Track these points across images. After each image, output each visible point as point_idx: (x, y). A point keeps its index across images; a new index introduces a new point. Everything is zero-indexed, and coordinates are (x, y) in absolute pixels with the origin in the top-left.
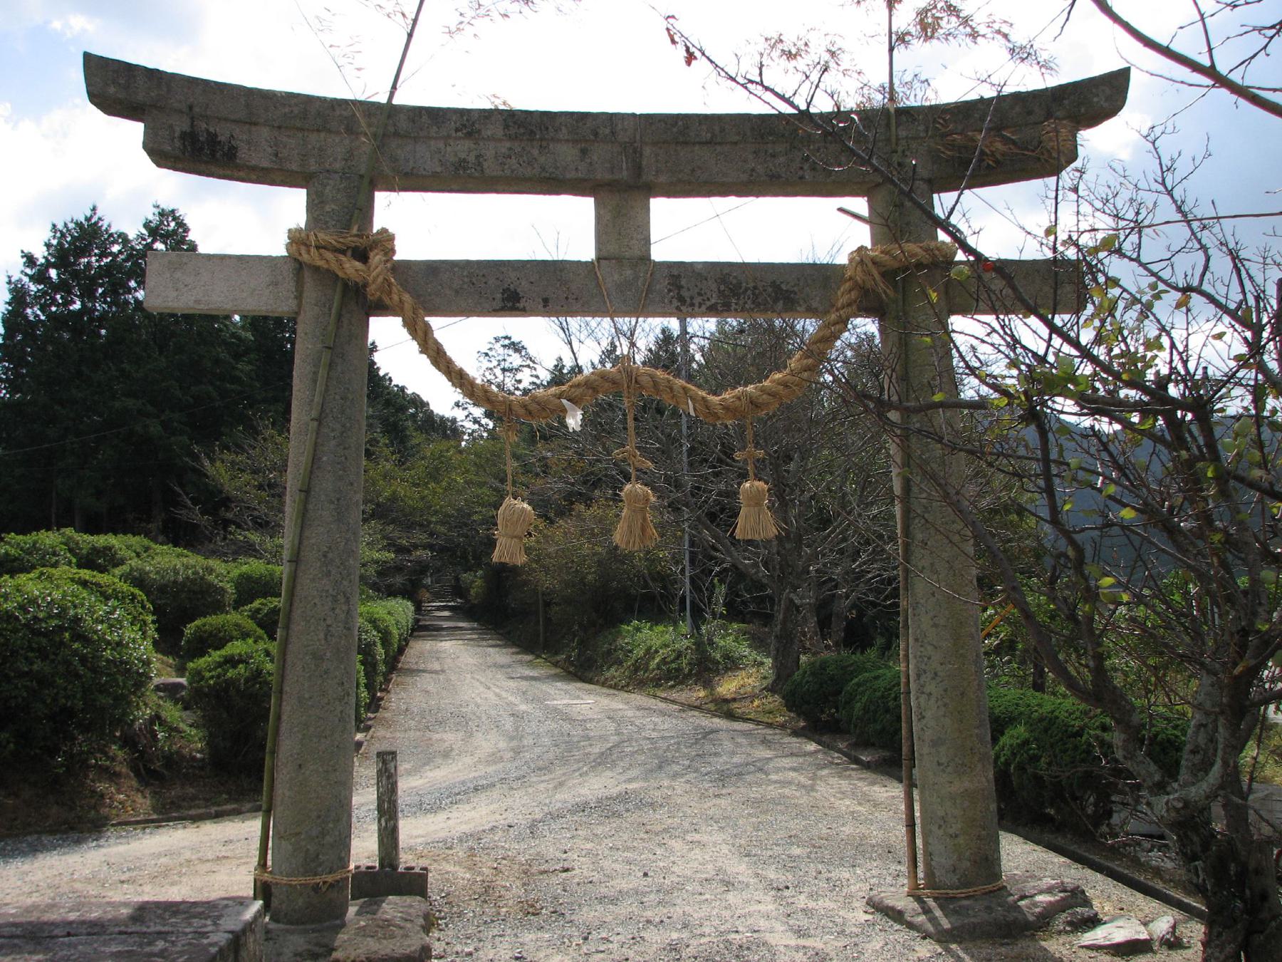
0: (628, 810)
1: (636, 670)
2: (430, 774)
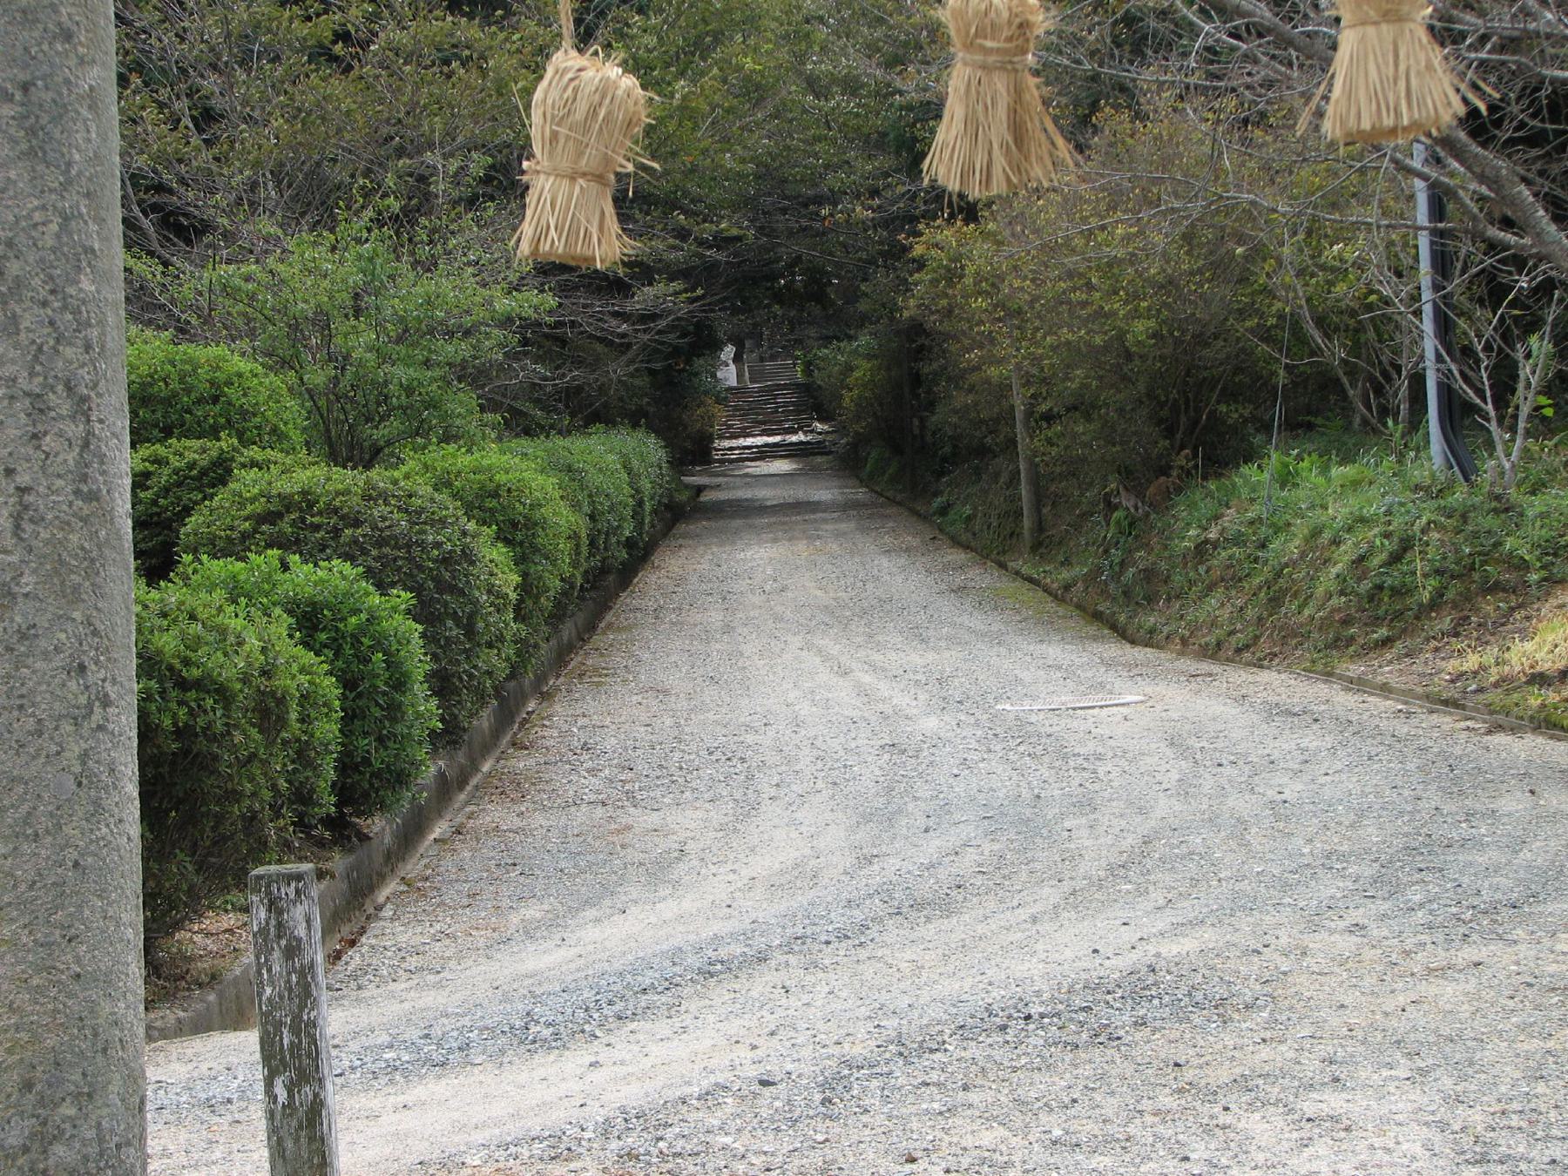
0: (1141, 1023)
1: (1275, 602)
2: (592, 933)
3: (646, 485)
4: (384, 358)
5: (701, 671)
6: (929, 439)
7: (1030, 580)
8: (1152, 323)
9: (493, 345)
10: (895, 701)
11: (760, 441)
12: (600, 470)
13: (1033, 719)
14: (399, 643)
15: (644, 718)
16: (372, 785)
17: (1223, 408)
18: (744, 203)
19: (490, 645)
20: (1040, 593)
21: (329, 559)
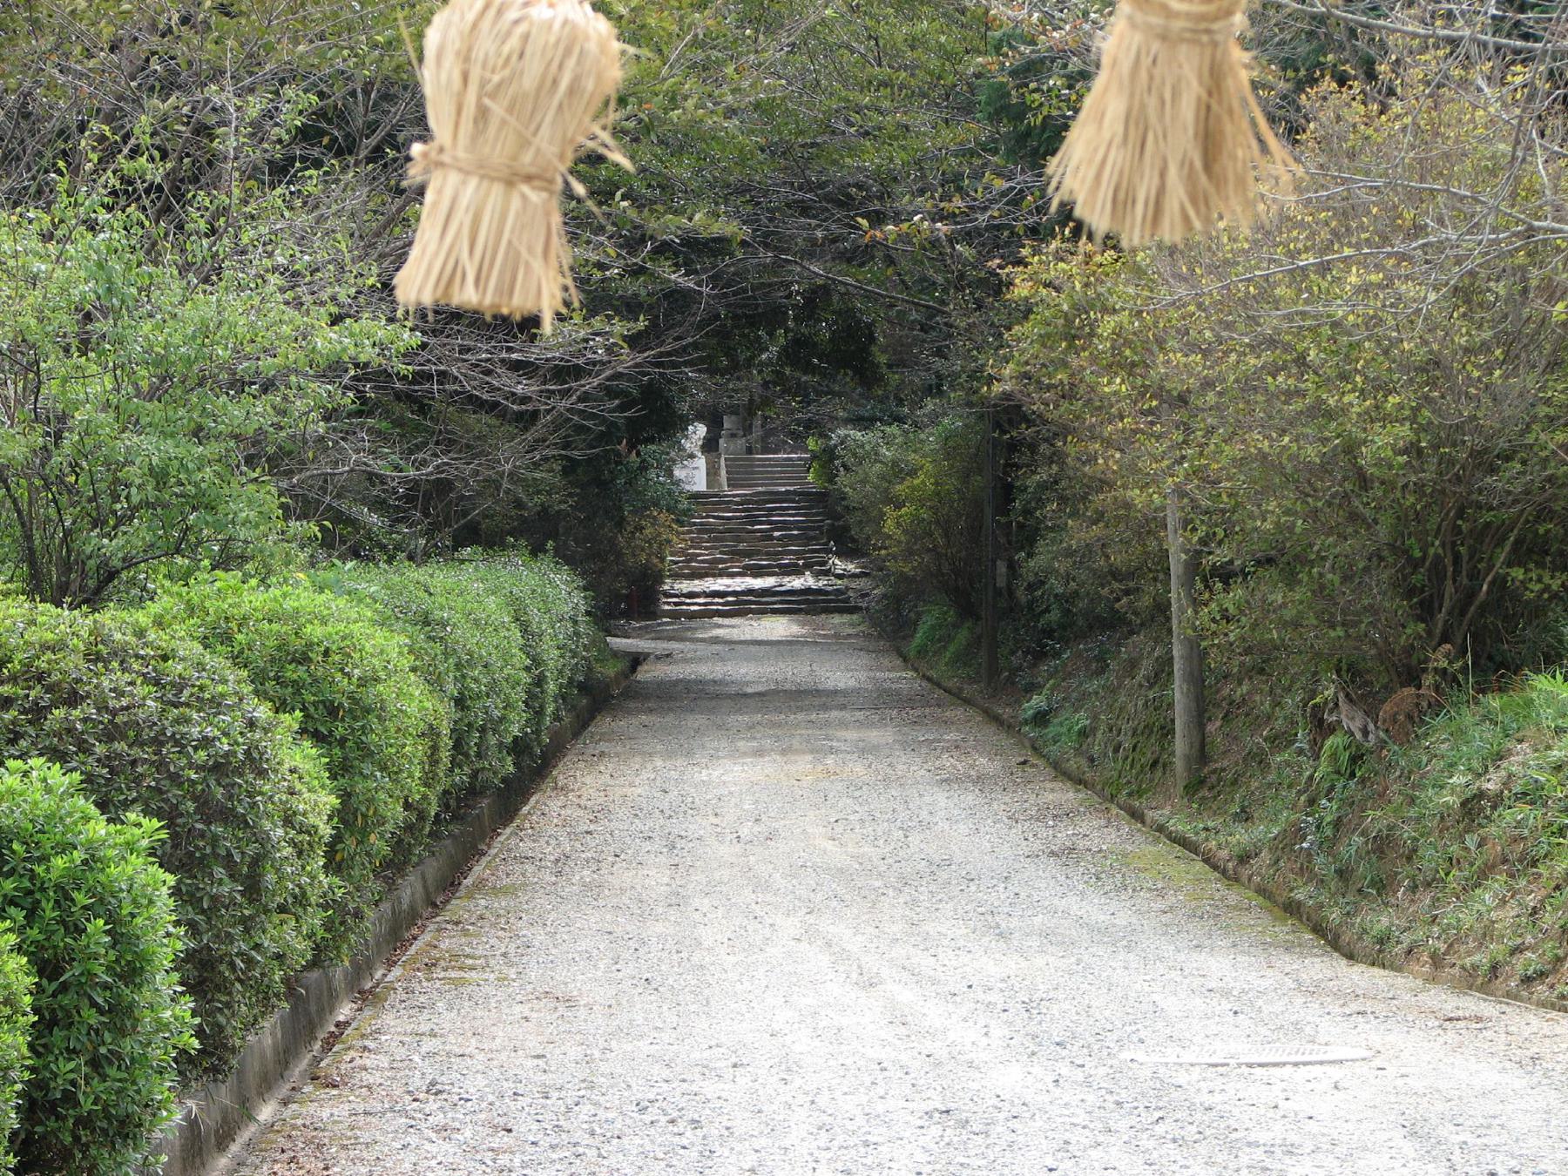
3: (551, 656)
4: (130, 423)
5: (629, 970)
6: (1022, 596)
7: (1182, 842)
8: (1404, 431)
9: (309, 403)
10: (952, 1036)
11: (740, 584)
12: (476, 622)
13: (1182, 1078)
14: (134, 902)
15: (533, 1044)
16: (77, 1139)
17: (1518, 573)
18: (734, 191)
19: (282, 909)
20: (1199, 866)
21: (23, 756)
